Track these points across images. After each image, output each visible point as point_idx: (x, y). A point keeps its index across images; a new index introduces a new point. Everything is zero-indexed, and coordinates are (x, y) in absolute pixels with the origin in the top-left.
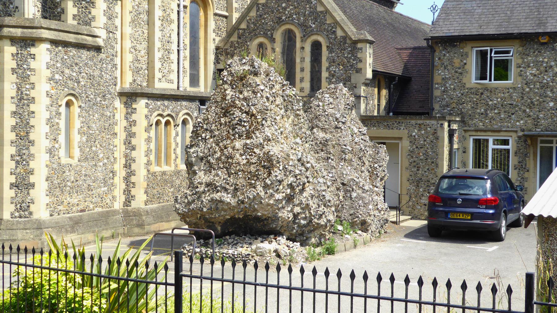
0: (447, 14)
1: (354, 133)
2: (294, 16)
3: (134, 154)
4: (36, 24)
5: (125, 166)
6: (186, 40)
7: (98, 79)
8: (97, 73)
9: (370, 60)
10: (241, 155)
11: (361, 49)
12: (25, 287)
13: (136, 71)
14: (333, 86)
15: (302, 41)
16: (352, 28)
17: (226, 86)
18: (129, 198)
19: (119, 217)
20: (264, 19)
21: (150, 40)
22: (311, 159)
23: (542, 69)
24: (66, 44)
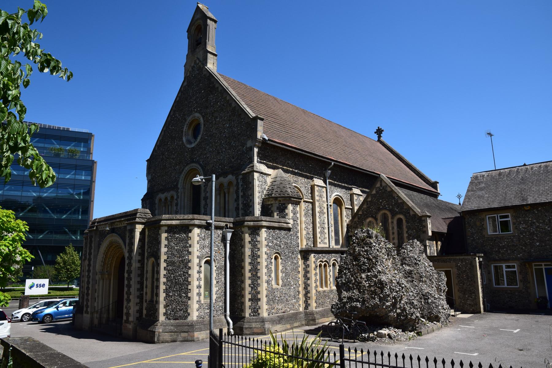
0: (469, 199)
1: (426, 266)
3: (309, 282)
4: (260, 219)
5: (305, 288)
6: (332, 222)
7: (290, 244)
9: (429, 226)
10: (366, 281)
11: (424, 220)
12: (258, 361)
13: (308, 239)
14: (411, 241)
16: (418, 209)
17: (355, 245)
18: (307, 305)
19: (302, 315)
21: (314, 223)
22: (403, 281)
24: (274, 228)
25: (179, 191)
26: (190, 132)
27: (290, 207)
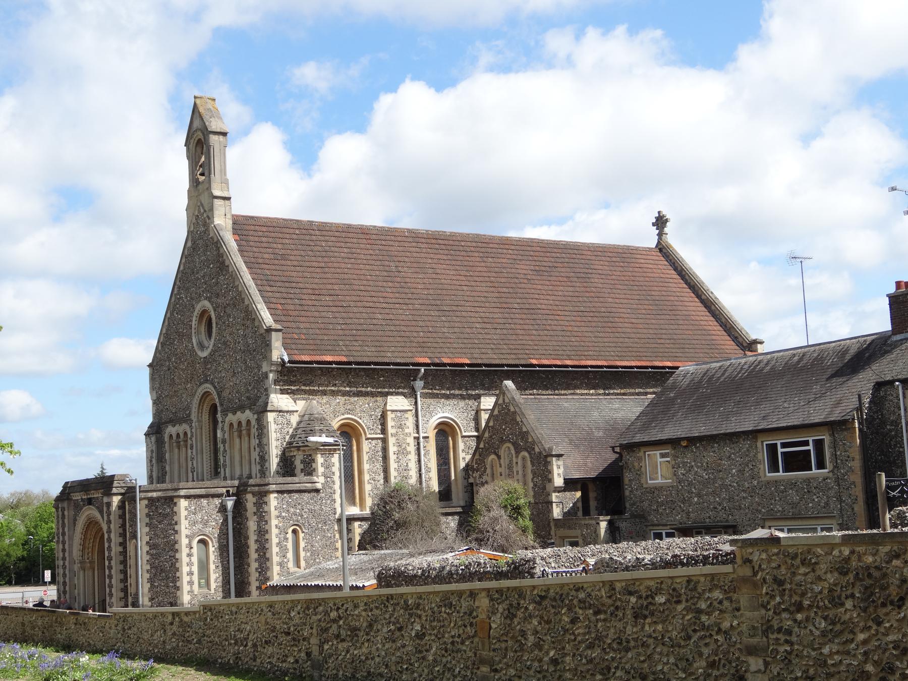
8: (317, 508)
25: (193, 425)
26: (203, 329)
27: (320, 459)
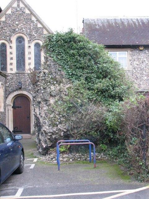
2: (24, 29)
15: (29, 43)
20: (4, 29)
23: (141, 62)
